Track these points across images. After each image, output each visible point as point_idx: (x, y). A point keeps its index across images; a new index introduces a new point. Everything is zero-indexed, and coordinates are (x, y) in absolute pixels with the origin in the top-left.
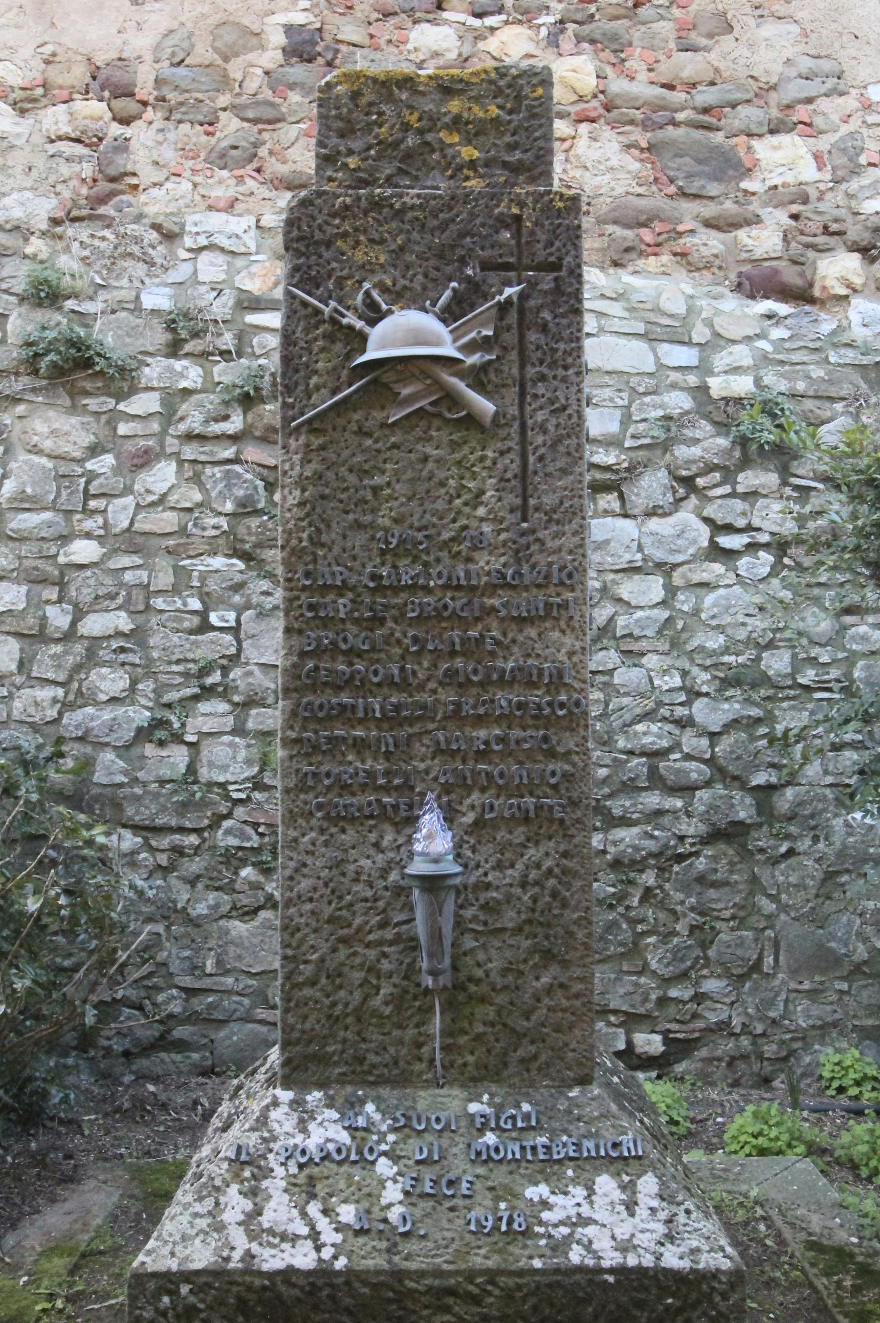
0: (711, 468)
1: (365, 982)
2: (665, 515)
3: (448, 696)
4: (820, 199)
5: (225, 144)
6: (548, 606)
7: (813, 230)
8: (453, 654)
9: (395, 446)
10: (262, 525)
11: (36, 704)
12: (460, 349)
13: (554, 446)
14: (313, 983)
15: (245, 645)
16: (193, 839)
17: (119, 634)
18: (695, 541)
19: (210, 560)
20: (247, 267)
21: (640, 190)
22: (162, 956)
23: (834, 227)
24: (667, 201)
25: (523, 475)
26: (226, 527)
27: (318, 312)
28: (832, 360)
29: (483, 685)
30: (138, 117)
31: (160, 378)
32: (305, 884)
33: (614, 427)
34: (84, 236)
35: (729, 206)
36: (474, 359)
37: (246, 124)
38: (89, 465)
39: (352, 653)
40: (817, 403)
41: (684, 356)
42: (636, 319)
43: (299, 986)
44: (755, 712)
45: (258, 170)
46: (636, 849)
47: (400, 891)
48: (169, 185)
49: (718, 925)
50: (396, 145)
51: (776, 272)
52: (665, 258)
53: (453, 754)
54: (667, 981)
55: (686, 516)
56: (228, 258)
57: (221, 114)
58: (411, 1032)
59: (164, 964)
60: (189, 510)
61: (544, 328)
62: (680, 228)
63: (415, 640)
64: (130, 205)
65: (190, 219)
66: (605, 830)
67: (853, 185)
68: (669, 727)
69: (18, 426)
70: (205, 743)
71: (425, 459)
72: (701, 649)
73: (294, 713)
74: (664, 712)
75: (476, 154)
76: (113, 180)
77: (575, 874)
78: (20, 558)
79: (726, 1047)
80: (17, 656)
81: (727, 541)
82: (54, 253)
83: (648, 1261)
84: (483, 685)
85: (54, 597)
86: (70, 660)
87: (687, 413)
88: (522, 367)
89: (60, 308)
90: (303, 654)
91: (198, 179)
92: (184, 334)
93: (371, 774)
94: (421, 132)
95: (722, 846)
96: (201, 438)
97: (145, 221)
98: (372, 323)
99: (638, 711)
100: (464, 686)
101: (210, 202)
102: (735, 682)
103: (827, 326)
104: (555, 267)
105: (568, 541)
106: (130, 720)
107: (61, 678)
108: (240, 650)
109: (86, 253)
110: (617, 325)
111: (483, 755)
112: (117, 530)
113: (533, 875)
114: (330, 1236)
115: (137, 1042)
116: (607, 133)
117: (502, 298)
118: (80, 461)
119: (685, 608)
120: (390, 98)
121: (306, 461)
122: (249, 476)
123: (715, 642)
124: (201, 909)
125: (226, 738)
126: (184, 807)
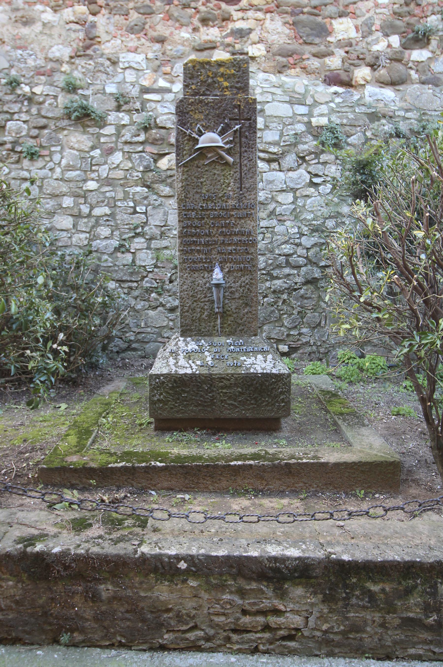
0: (311, 153)
1: (201, 311)
2: (294, 170)
3: (221, 238)
4: (357, 45)
5: (132, 24)
6: (247, 214)
7: (353, 58)
8: (222, 227)
9: (207, 171)
10: (153, 175)
11: (80, 239)
12: (224, 144)
13: (249, 171)
14: (188, 311)
15: (149, 218)
16: (135, 284)
17: (106, 215)
18: (304, 180)
19: (136, 188)
20: (143, 75)
21: (289, 42)
22: (127, 322)
23: (361, 56)
24: (299, 46)
25: (241, 179)
26: (141, 176)
27: (185, 133)
28: (357, 111)
29: (230, 235)
30: (99, 12)
31: (114, 120)
32: (185, 287)
33: (277, 138)
34: (83, 63)
35: (323, 47)
36: (227, 146)
37: (140, 15)
38: (92, 154)
39: (196, 227)
40: (350, 128)
41: (302, 110)
42: (286, 95)
43: (184, 312)
44: (322, 241)
45: (145, 35)
46: (281, 287)
47: (210, 289)
48: (112, 41)
49: (307, 311)
50: (205, 82)
51: (338, 75)
52: (298, 70)
53: (222, 253)
54: (290, 329)
55: (302, 171)
56: (136, 72)
57: (131, 12)
58: (213, 323)
59: (128, 324)
60: (128, 170)
61: (246, 137)
62: (304, 57)
63: (213, 223)
64: (98, 50)
65: (121, 56)
66: (271, 281)
67: (369, 39)
68: (293, 246)
69: (65, 139)
70: (137, 252)
71: (215, 174)
72: (305, 219)
73: (181, 243)
74: (292, 241)
75: (228, 84)
76: (91, 39)
77: (254, 284)
78: (70, 188)
79: (308, 349)
80: (72, 223)
81: (316, 180)
82: (72, 70)
83: (269, 371)
84: (230, 235)
85: (83, 202)
86: (90, 224)
87: (303, 132)
88: (240, 148)
89: (77, 94)
90: (183, 227)
91: (123, 39)
92: (122, 103)
93: (201, 259)
94: (212, 78)
95: (309, 286)
96: (130, 143)
97: (104, 56)
98: (200, 136)
99: (283, 241)
100: (225, 235)
101: (128, 48)
102: (316, 231)
103: (356, 97)
104: (250, 119)
105: (253, 197)
106: (112, 245)
107: (88, 230)
108: (147, 220)
109: (84, 70)
110: (279, 98)
111: (230, 254)
112: (103, 178)
113: (243, 284)
114: (194, 367)
115: (120, 348)
116: (277, 17)
117: (235, 129)
118: (88, 152)
119: (300, 204)
120: (204, 68)
121: (183, 175)
122: (148, 157)
123: (310, 216)
124: (139, 307)
125: (144, 251)
126: (132, 274)
